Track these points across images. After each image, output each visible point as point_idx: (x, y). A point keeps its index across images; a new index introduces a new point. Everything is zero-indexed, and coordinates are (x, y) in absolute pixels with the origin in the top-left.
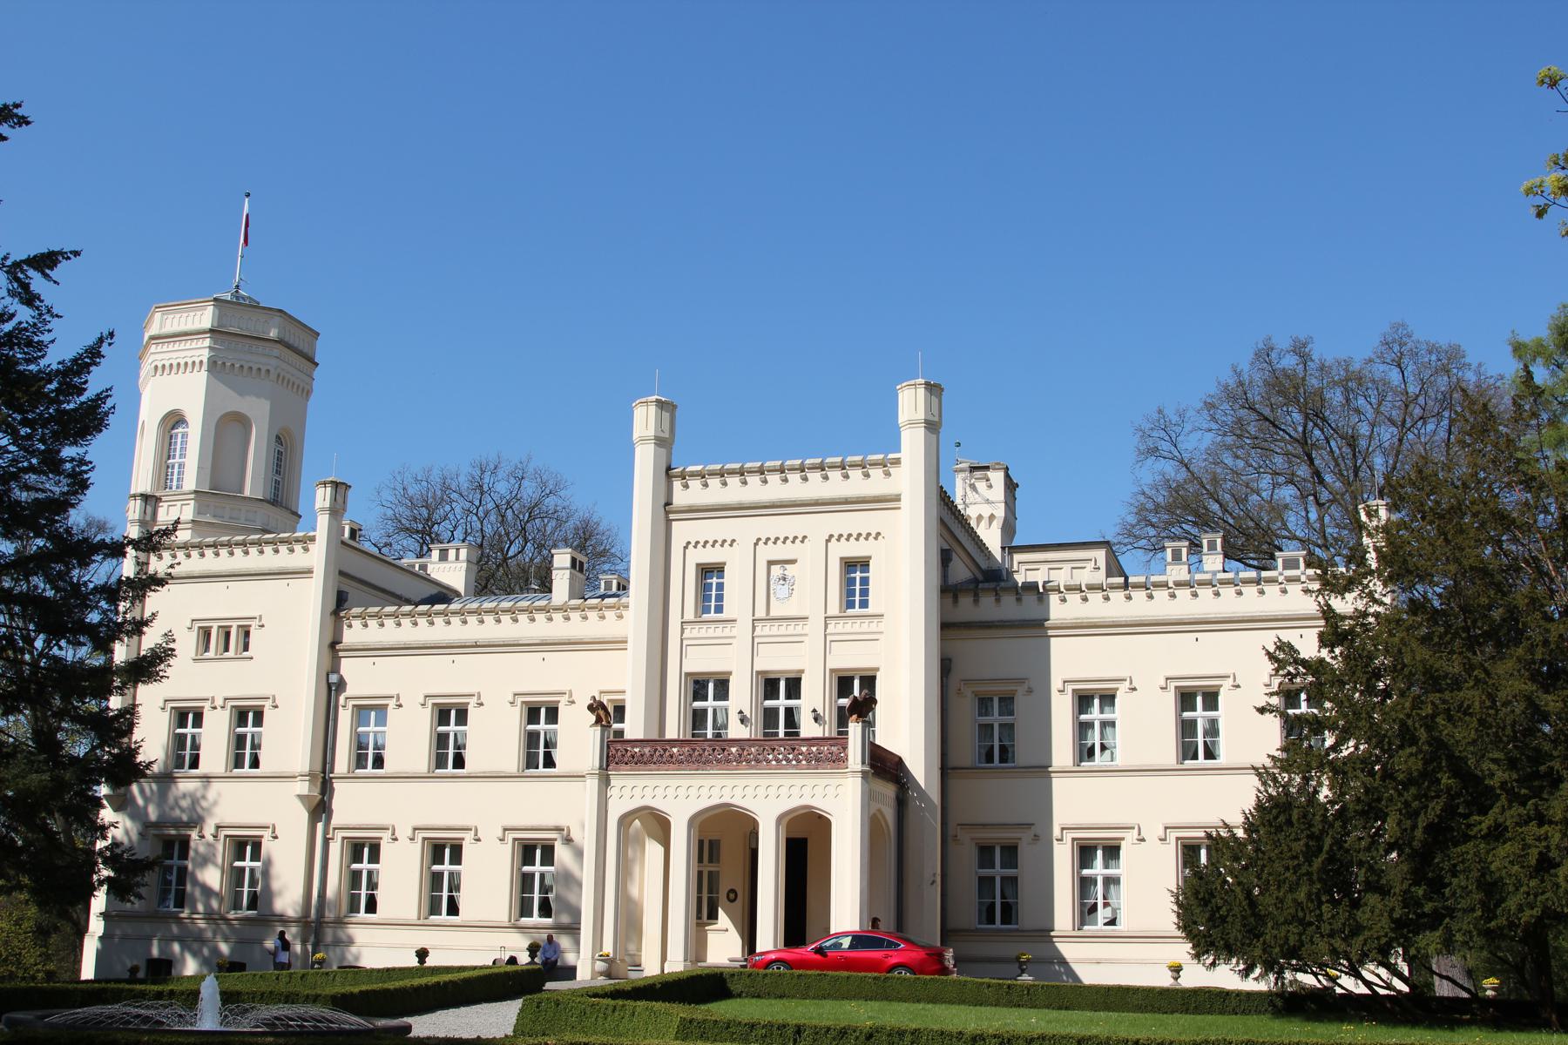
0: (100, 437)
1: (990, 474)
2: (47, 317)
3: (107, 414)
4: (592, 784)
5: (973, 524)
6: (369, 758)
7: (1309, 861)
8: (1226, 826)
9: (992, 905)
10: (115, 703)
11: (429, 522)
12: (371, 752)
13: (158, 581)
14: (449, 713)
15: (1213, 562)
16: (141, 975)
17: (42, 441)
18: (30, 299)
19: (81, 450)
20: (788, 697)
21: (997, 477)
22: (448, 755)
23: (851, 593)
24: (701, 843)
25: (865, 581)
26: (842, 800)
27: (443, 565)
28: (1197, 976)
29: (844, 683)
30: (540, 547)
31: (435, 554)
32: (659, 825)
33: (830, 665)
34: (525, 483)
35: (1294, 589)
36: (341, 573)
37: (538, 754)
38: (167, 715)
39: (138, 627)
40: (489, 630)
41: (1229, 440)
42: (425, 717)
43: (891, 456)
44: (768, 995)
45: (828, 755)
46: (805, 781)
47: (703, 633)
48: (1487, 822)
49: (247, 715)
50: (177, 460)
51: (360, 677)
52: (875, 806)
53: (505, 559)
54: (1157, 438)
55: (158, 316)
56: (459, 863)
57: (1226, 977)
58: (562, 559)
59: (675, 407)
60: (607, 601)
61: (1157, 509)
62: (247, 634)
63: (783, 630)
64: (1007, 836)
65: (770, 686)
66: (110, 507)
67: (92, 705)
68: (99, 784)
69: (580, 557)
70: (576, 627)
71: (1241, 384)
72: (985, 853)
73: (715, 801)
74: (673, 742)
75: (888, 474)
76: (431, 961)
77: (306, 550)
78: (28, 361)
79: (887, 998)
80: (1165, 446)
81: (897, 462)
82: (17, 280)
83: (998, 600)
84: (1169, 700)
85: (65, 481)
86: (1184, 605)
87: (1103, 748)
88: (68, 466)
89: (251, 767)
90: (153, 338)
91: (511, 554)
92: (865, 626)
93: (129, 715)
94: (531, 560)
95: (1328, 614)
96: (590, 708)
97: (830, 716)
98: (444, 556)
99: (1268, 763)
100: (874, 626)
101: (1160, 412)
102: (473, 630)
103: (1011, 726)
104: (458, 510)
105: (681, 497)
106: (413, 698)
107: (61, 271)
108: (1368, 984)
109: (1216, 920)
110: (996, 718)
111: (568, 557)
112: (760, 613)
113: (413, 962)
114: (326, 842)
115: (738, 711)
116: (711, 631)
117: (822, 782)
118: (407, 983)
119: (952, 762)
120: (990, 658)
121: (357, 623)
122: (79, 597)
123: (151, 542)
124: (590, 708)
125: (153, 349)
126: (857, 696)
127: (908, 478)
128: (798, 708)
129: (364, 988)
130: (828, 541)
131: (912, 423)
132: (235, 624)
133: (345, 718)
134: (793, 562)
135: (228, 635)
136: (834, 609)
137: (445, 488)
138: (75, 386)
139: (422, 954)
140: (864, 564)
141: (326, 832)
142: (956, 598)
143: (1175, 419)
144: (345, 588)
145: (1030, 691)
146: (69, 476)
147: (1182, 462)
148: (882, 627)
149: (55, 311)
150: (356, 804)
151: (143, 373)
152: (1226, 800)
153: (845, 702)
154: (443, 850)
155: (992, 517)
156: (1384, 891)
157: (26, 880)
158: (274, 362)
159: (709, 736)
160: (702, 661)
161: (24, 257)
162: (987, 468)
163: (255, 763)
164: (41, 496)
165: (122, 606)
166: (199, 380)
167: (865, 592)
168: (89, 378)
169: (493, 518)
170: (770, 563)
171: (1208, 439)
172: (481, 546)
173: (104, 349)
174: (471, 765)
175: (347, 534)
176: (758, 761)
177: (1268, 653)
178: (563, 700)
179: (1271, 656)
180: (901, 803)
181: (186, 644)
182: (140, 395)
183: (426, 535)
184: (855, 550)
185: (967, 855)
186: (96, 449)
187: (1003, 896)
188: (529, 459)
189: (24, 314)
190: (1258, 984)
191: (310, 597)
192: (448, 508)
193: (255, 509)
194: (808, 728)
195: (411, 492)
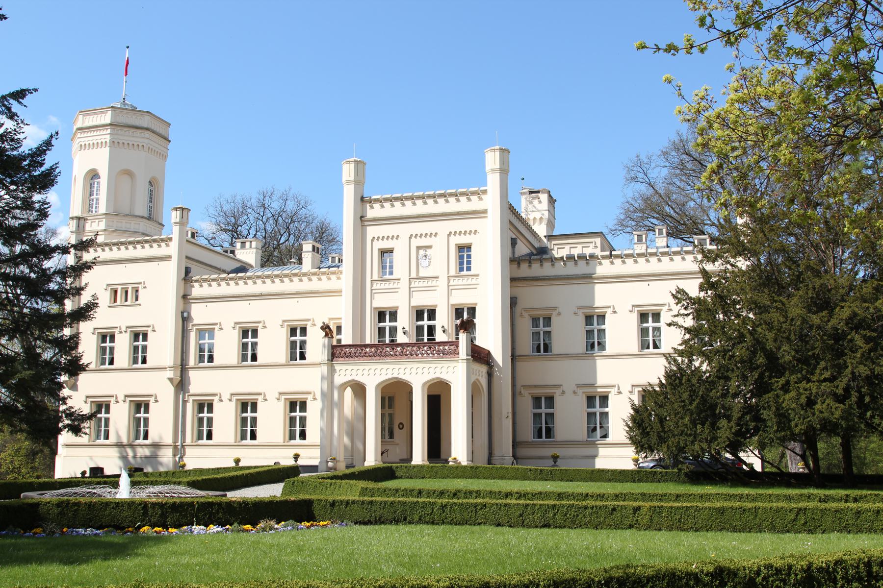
0: (53, 188)
1: (540, 195)
2: (22, 125)
3: (56, 176)
4: (325, 369)
5: (531, 223)
6: (207, 356)
7: (691, 404)
8: (650, 385)
9: (541, 428)
10: (67, 332)
11: (236, 226)
12: (206, 354)
13: (87, 266)
14: (248, 332)
15: (661, 242)
17: (23, 192)
18: (12, 116)
19: (44, 196)
20: (429, 319)
21: (544, 197)
22: (249, 354)
23: (461, 263)
24: (383, 399)
25: (469, 257)
26: (456, 374)
27: (243, 251)
29: (459, 312)
30: (297, 238)
31: (238, 245)
32: (359, 390)
33: (451, 302)
34: (288, 202)
35: (689, 258)
36: (187, 257)
37: (297, 352)
38: (95, 337)
39: (78, 291)
40: (269, 287)
41: (678, 171)
42: (236, 335)
43: (482, 188)
44: (416, 477)
46: (437, 365)
47: (383, 286)
48: (782, 381)
49: (139, 335)
50: (95, 196)
51: (200, 314)
52: (473, 379)
53: (279, 245)
54: (636, 172)
55: (81, 117)
56: (305, 411)
58: (307, 247)
59: (365, 164)
60: (331, 269)
61: (636, 210)
62: (137, 291)
63: (425, 284)
64: (549, 391)
65: (419, 314)
66: (59, 230)
67: (55, 334)
68: (61, 375)
69: (317, 245)
70: (315, 284)
71: (681, 141)
72: (537, 401)
73: (389, 376)
74: (367, 346)
75: (480, 199)
76: (241, 464)
77: (167, 245)
78: (13, 149)
79: (478, 477)
80: (641, 176)
81: (485, 192)
82: (4, 105)
83: (542, 265)
84: (634, 318)
85: (36, 214)
87: (599, 343)
88: (37, 205)
90: (79, 129)
91: (281, 242)
93: (74, 340)
94: (293, 244)
95: (705, 273)
96: (322, 328)
97: (452, 330)
99: (672, 351)
101: (638, 157)
102: (259, 287)
104: (251, 218)
105: (371, 213)
106: (228, 325)
107: (28, 99)
109: (645, 433)
110: (542, 329)
111: (311, 246)
112: (414, 275)
113: (234, 465)
114: (185, 402)
116: (387, 285)
117: (446, 365)
118: (227, 475)
119: (519, 352)
120: (537, 297)
121: (196, 285)
122: (46, 276)
123: (83, 246)
124: (322, 328)
125: (79, 135)
126: (466, 320)
127: (492, 202)
128: (434, 326)
129: (204, 477)
130: (449, 235)
131: (493, 170)
132: (130, 287)
133: (193, 336)
134: (430, 247)
135: (127, 292)
136: (453, 272)
137: (244, 206)
138: (38, 162)
139: (237, 461)
140: (469, 247)
141: (184, 397)
142: (519, 264)
143: (646, 161)
144: (189, 265)
145: (559, 314)
146: (37, 211)
147: (650, 184)
148: (478, 281)
150: (201, 382)
151: (74, 150)
152: (653, 371)
154: (247, 406)
155: (541, 218)
156: (729, 418)
157: (24, 426)
158: (146, 141)
159: (387, 342)
160: (383, 302)
161: (8, 93)
162: (538, 192)
163: (144, 361)
164: (22, 222)
165: (69, 281)
166: (108, 137)
167: (469, 263)
168: (46, 157)
169: (271, 221)
170: (419, 248)
171: (665, 172)
172: (265, 238)
173: (54, 141)
174: (261, 359)
175: (190, 235)
176: (412, 355)
178: (309, 324)
179: (674, 296)
180: (490, 375)
181: (104, 299)
182: (72, 161)
183: (234, 232)
184: (463, 240)
186: (52, 196)
187: (546, 423)
188: (290, 189)
189: (9, 124)
191: (170, 272)
192: (246, 217)
193: (140, 219)
194: (440, 337)
195: (225, 208)
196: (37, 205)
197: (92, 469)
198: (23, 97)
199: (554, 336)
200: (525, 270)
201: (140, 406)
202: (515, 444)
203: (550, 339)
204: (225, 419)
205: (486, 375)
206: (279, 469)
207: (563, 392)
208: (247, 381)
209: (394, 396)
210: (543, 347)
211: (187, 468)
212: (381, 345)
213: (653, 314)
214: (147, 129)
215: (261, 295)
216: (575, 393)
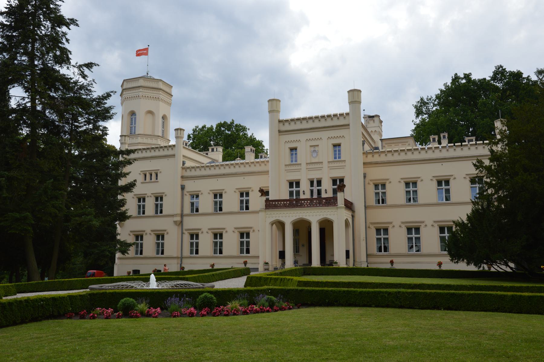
6: (195, 209)
14: (218, 195)
15: (445, 142)
16: (131, 274)
18: (84, 76)
22: (219, 208)
27: (213, 153)
28: (449, 265)
29: (334, 182)
31: (210, 150)
37: (245, 206)
45: (331, 202)
49: (159, 198)
56: (299, 187)
57: (462, 266)
76: (215, 267)
82: (80, 70)
86: (438, 154)
89: (220, 254)
92: (297, 167)
96: (259, 191)
100: (343, 164)
103: (416, 191)
107: (94, 68)
108: (511, 268)
110: (380, 191)
115: (305, 189)
134: (318, 146)
139: (213, 266)
149: (95, 81)
152: (461, 213)
153: (336, 187)
154: (218, 235)
167: (340, 154)
174: (224, 210)
177: (473, 164)
185: (373, 233)
190: (472, 268)
196: (101, 128)
197: (133, 271)
198: (91, 67)
199: (388, 195)
200: (370, 159)
201: (160, 236)
202: (368, 256)
203: (417, 195)
204: (206, 244)
205: (351, 217)
206: (393, 270)
207: (254, 231)
208: (412, 215)
209: (302, 230)
210: (381, 200)
211: (185, 270)
213: (413, 183)
214: (139, 87)
215: (224, 175)
216: (432, 225)
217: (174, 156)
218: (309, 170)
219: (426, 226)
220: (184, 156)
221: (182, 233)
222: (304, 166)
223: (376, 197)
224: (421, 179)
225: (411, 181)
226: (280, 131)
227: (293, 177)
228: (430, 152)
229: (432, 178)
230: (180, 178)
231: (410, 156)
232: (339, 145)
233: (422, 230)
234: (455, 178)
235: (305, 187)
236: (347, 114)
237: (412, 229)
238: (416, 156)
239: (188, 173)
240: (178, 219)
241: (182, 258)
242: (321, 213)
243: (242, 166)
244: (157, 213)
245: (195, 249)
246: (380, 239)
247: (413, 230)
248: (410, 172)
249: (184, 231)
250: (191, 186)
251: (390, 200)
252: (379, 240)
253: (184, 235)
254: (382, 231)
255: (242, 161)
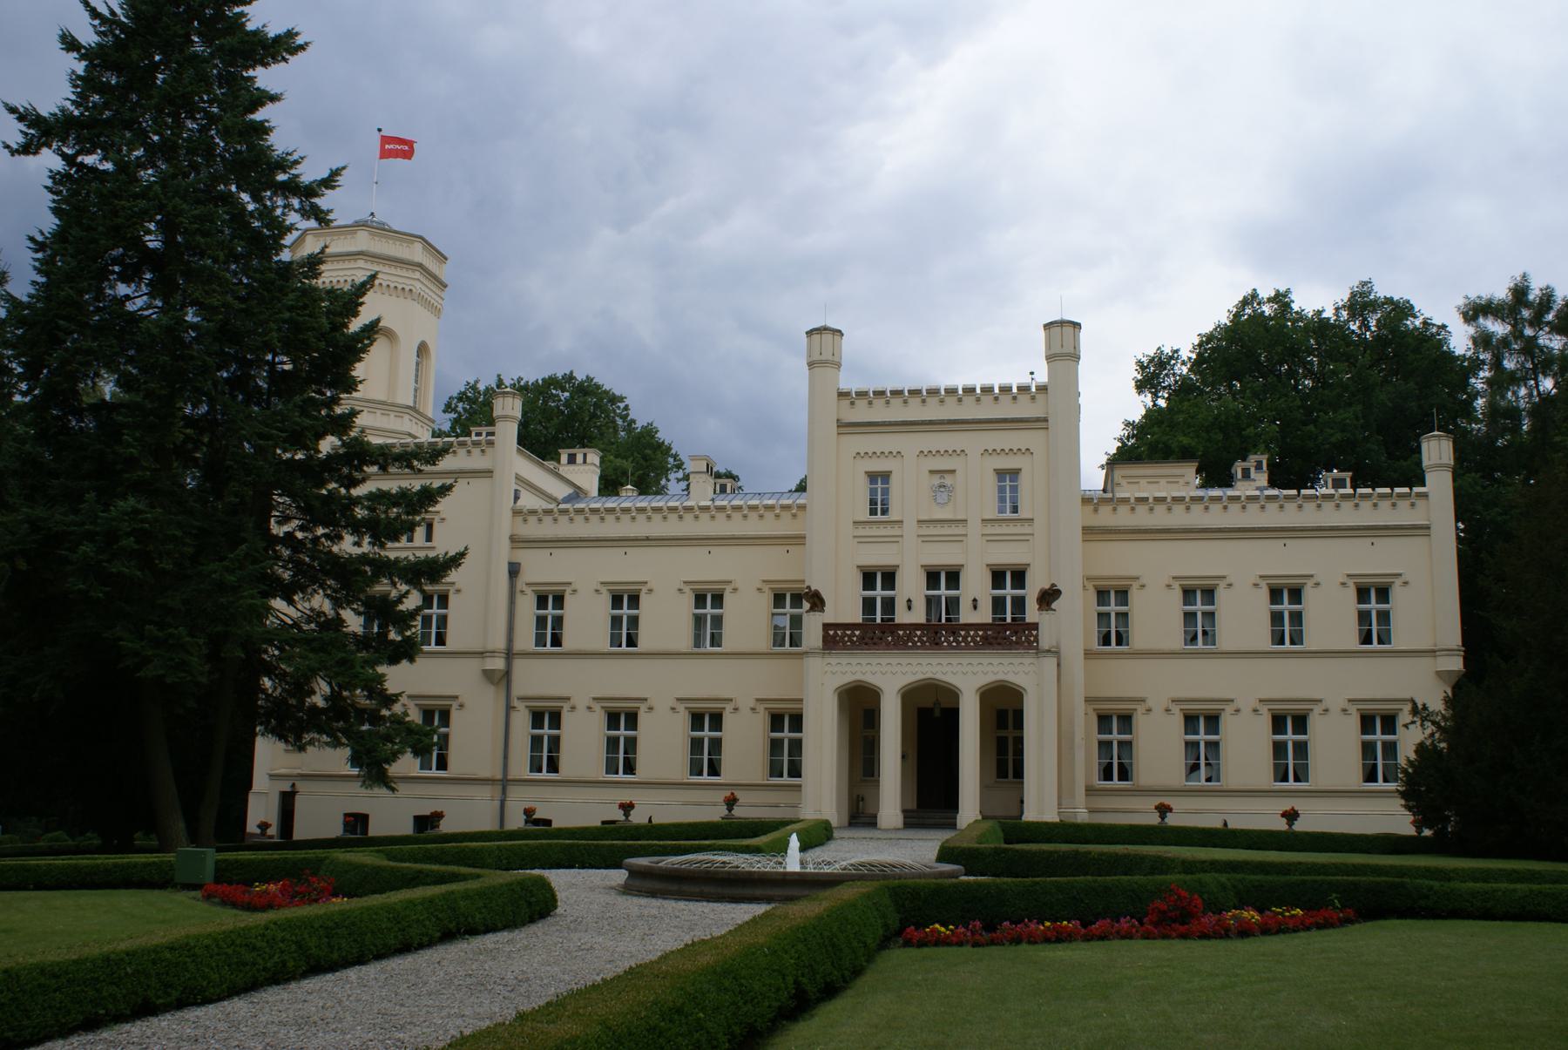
14: (625, 598)
22: (625, 634)
27: (571, 467)
31: (564, 458)
87: (1205, 633)
92: (889, 531)
98: (572, 460)
100: (1026, 529)
103: (1125, 615)
115: (911, 592)
134: (953, 472)
154: (622, 717)
158: (419, 285)
204: (583, 742)
207: (573, 708)
210: (551, 634)
212: (998, 626)
215: (647, 539)
216: (1255, 711)
217: (488, 473)
218: (926, 539)
219: (1238, 711)
220: (518, 477)
221: (509, 708)
222: (910, 528)
223: (1360, 624)
224: (1228, 581)
225: (1198, 586)
226: (841, 424)
227: (878, 557)
228: (1235, 508)
229: (1345, 579)
230: (506, 542)
231: (1179, 518)
232: (1015, 473)
233: (1226, 721)
234: (735, 590)
235: (911, 587)
236: (1042, 389)
237: (1197, 718)
238: (1197, 518)
239: (532, 529)
240: (498, 664)
241: (505, 783)
242: (990, 668)
243: (657, 517)
244: (698, 641)
245: (547, 756)
246: (1110, 743)
247: (1202, 721)
248: (1199, 560)
249: (516, 703)
250: (541, 569)
251: (1140, 636)
252: (1105, 746)
253: (514, 716)
254: (1115, 720)
255: (643, 502)
